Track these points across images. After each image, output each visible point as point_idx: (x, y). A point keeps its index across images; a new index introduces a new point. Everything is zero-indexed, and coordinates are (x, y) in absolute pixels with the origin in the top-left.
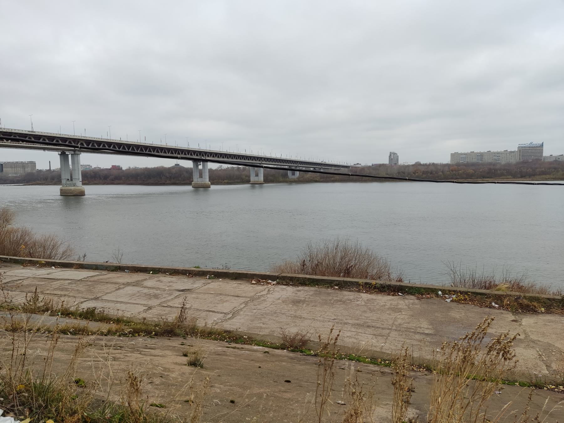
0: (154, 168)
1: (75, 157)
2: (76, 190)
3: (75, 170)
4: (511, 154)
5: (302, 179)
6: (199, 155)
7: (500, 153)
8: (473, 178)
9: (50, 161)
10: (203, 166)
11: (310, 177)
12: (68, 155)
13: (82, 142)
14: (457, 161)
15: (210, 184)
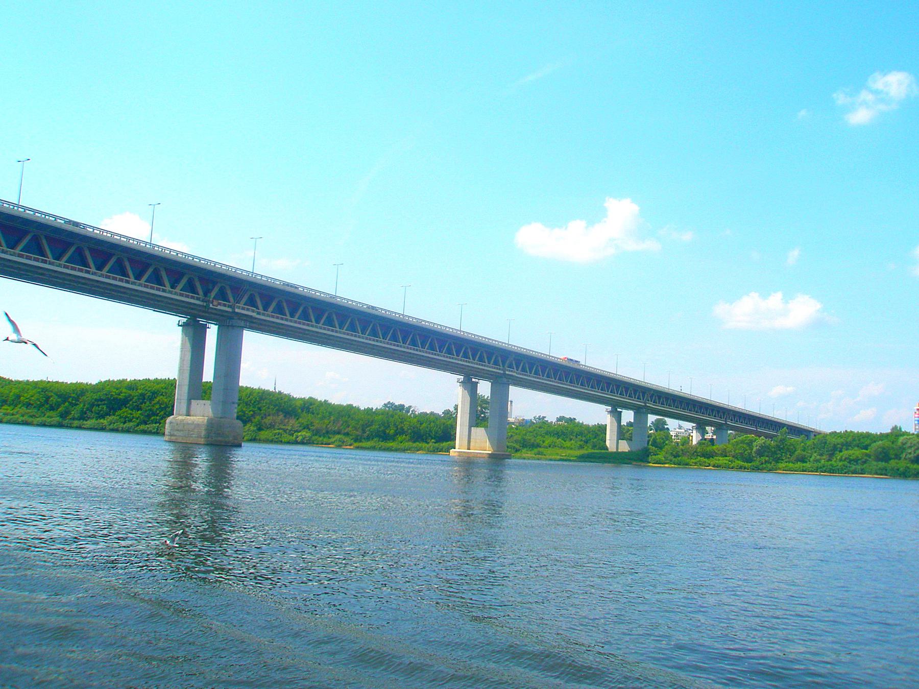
6: (577, 381)
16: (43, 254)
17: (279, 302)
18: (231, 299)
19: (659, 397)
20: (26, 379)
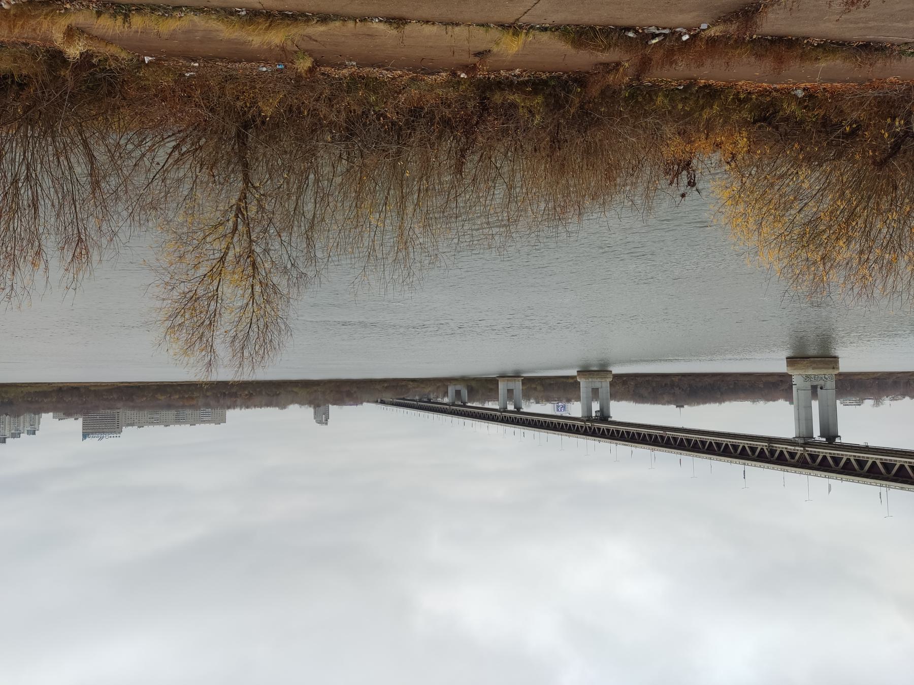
0: (705, 402)
1: (804, 431)
2: (803, 369)
3: (805, 407)
4: (132, 422)
5: (438, 385)
6: (579, 428)
7: (149, 423)
8: (155, 387)
10: (589, 409)
11: (424, 388)
12: (821, 436)
13: (792, 460)
14: (216, 411)
15: (578, 377)
16: (882, 463)
17: (736, 452)
18: (806, 455)
19: (468, 415)
20: (358, 406)
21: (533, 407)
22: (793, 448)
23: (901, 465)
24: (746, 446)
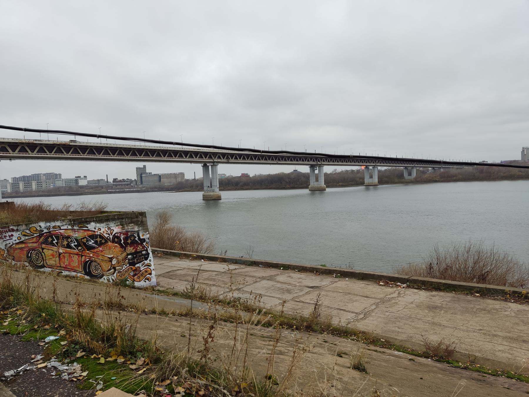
1: (214, 168)
9: (107, 175)
10: (319, 171)
11: (429, 177)
18: (213, 158)
21: (304, 169)
22: (218, 161)
23: (114, 155)
24: (239, 160)
